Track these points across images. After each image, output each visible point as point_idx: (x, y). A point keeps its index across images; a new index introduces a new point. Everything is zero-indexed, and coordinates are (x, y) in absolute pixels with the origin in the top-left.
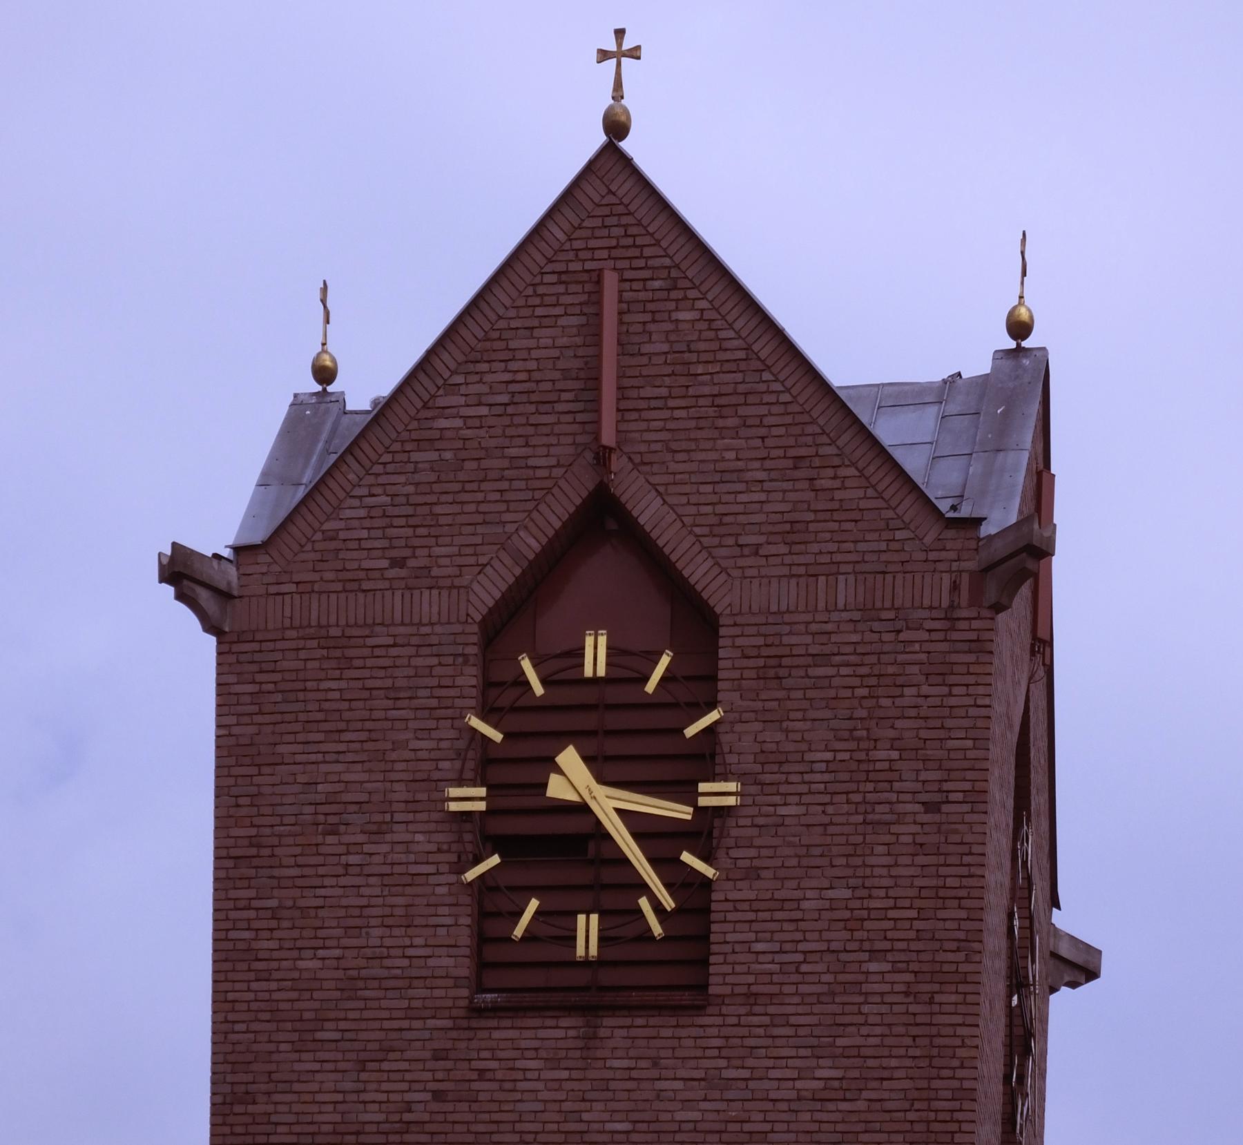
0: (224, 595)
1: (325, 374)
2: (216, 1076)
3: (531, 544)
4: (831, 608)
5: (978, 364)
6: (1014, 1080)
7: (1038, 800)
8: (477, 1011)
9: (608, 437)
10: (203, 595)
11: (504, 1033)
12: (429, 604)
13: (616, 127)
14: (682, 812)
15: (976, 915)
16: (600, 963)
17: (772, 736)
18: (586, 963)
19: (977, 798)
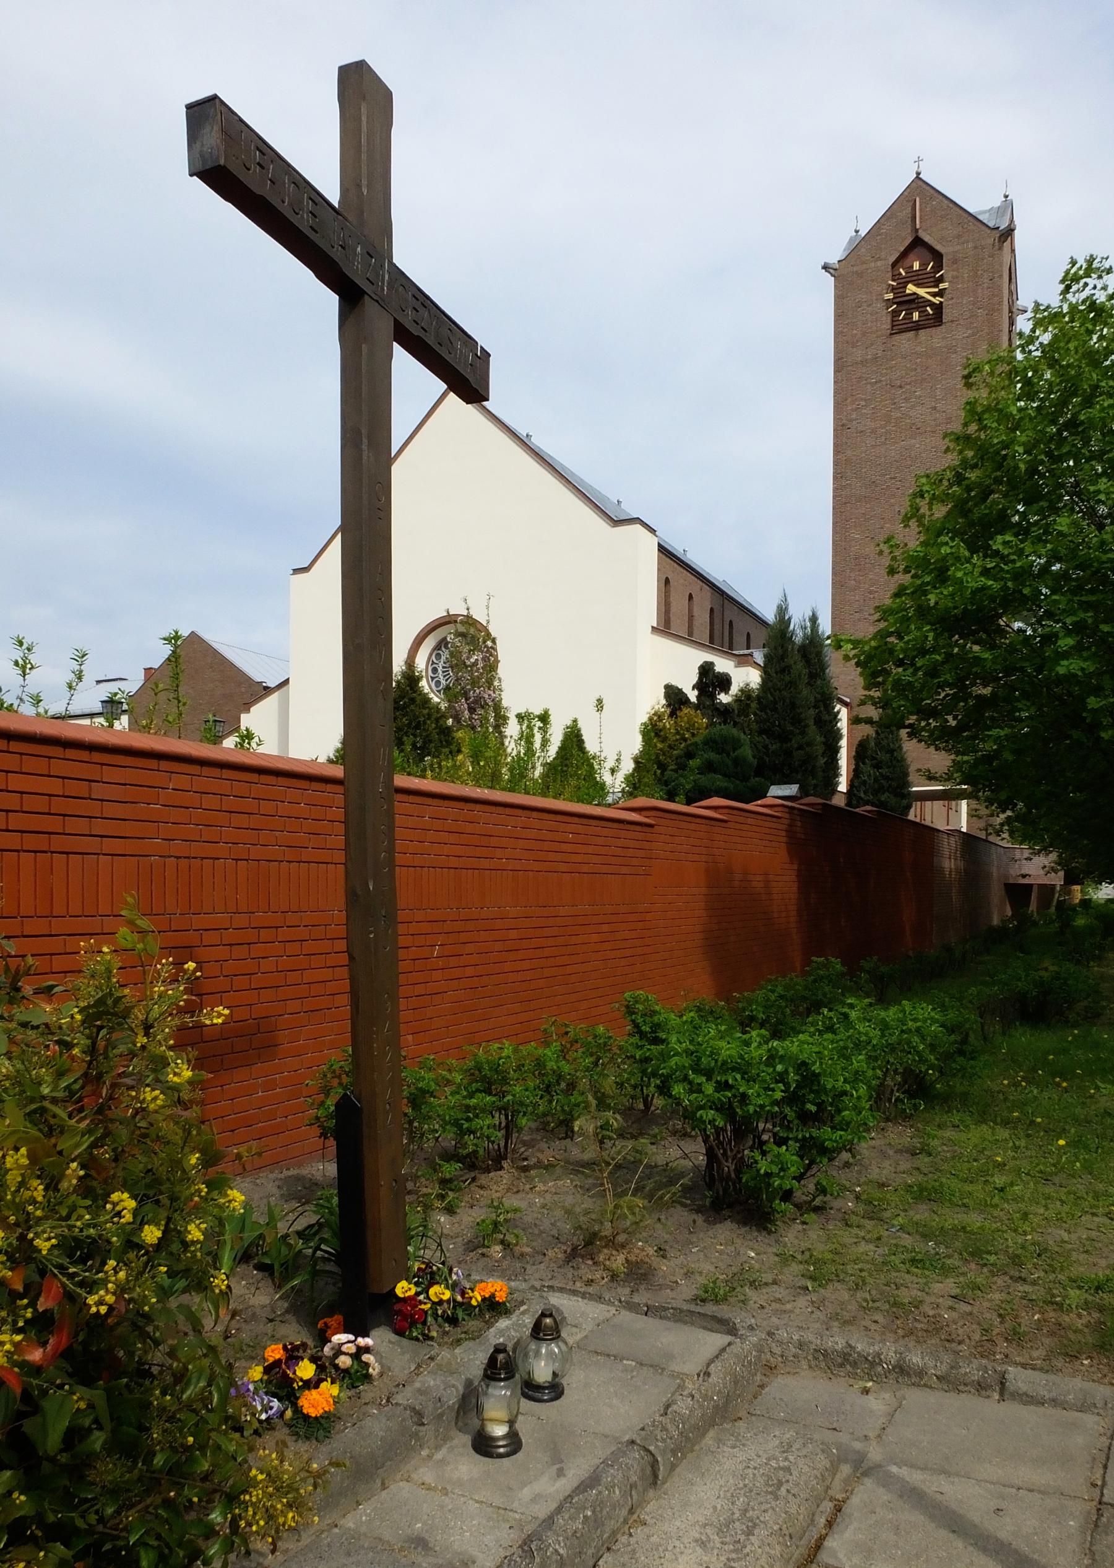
0: (836, 270)
1: (857, 232)
2: (191, 111)
3: (902, 249)
4: (967, 248)
5: (997, 204)
6: (941, 788)
7: (1013, 280)
8: (891, 334)
9: (918, 227)
10: (831, 271)
11: (897, 337)
12: (879, 263)
13: (918, 174)
14: (937, 290)
15: (1002, 298)
16: (918, 321)
17: (955, 273)
18: (916, 322)
19: (1001, 276)
